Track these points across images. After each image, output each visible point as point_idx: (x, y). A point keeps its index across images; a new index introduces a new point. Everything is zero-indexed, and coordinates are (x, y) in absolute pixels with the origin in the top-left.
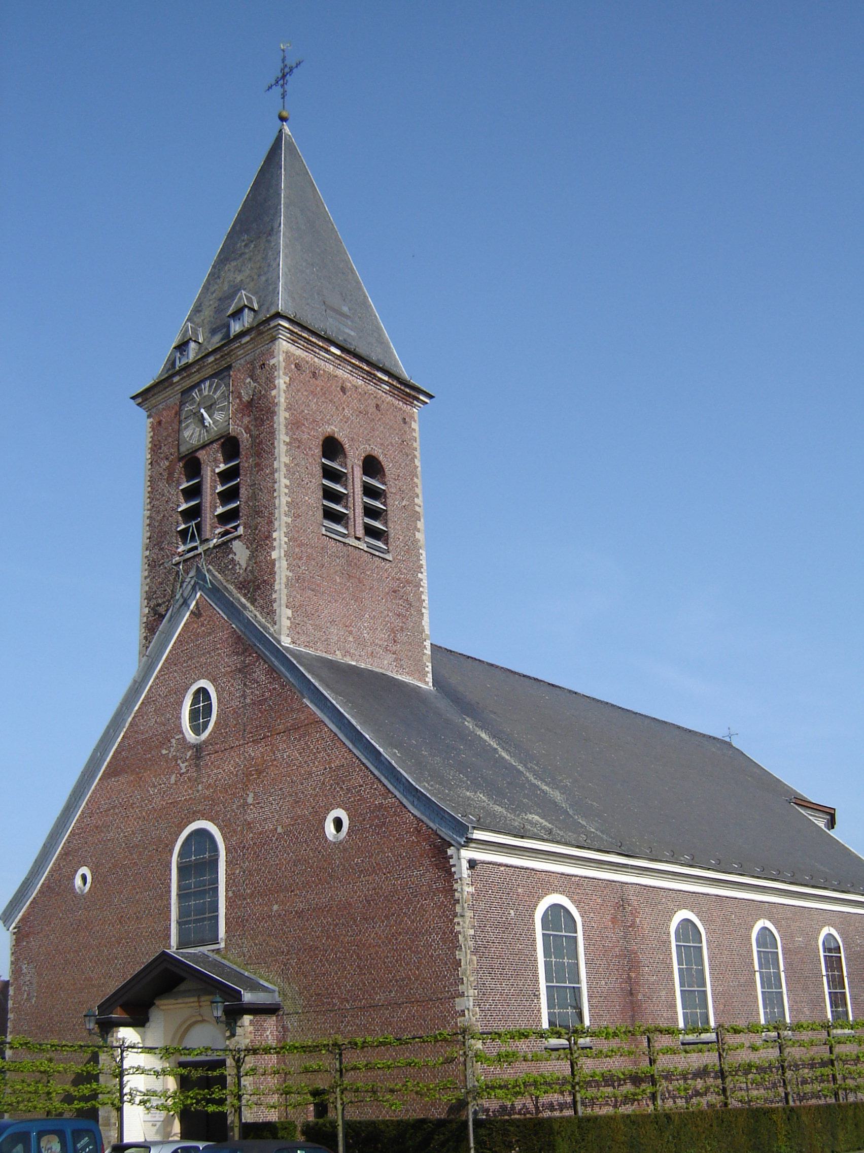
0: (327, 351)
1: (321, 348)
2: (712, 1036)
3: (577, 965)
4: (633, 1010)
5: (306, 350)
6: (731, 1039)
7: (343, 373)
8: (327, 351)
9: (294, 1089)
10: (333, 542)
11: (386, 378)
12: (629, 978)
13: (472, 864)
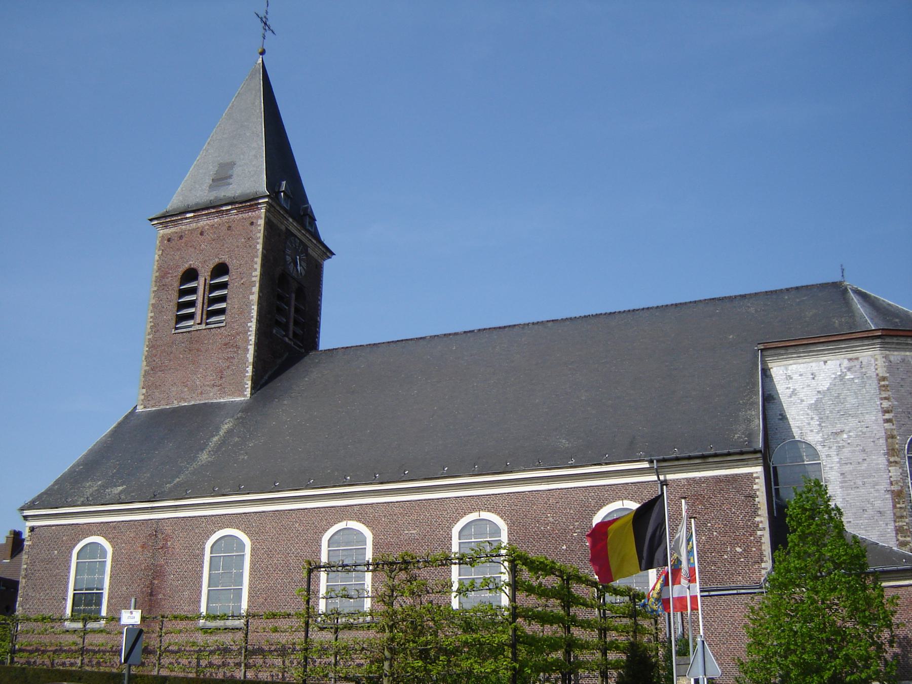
0: (186, 218)
1: (181, 219)
2: (240, 623)
3: (242, 574)
4: (150, 606)
5: (175, 226)
6: (254, 623)
7: (204, 223)
8: (186, 218)
9: (108, 648)
10: (180, 335)
11: (230, 207)
12: (152, 583)
13: (32, 529)
